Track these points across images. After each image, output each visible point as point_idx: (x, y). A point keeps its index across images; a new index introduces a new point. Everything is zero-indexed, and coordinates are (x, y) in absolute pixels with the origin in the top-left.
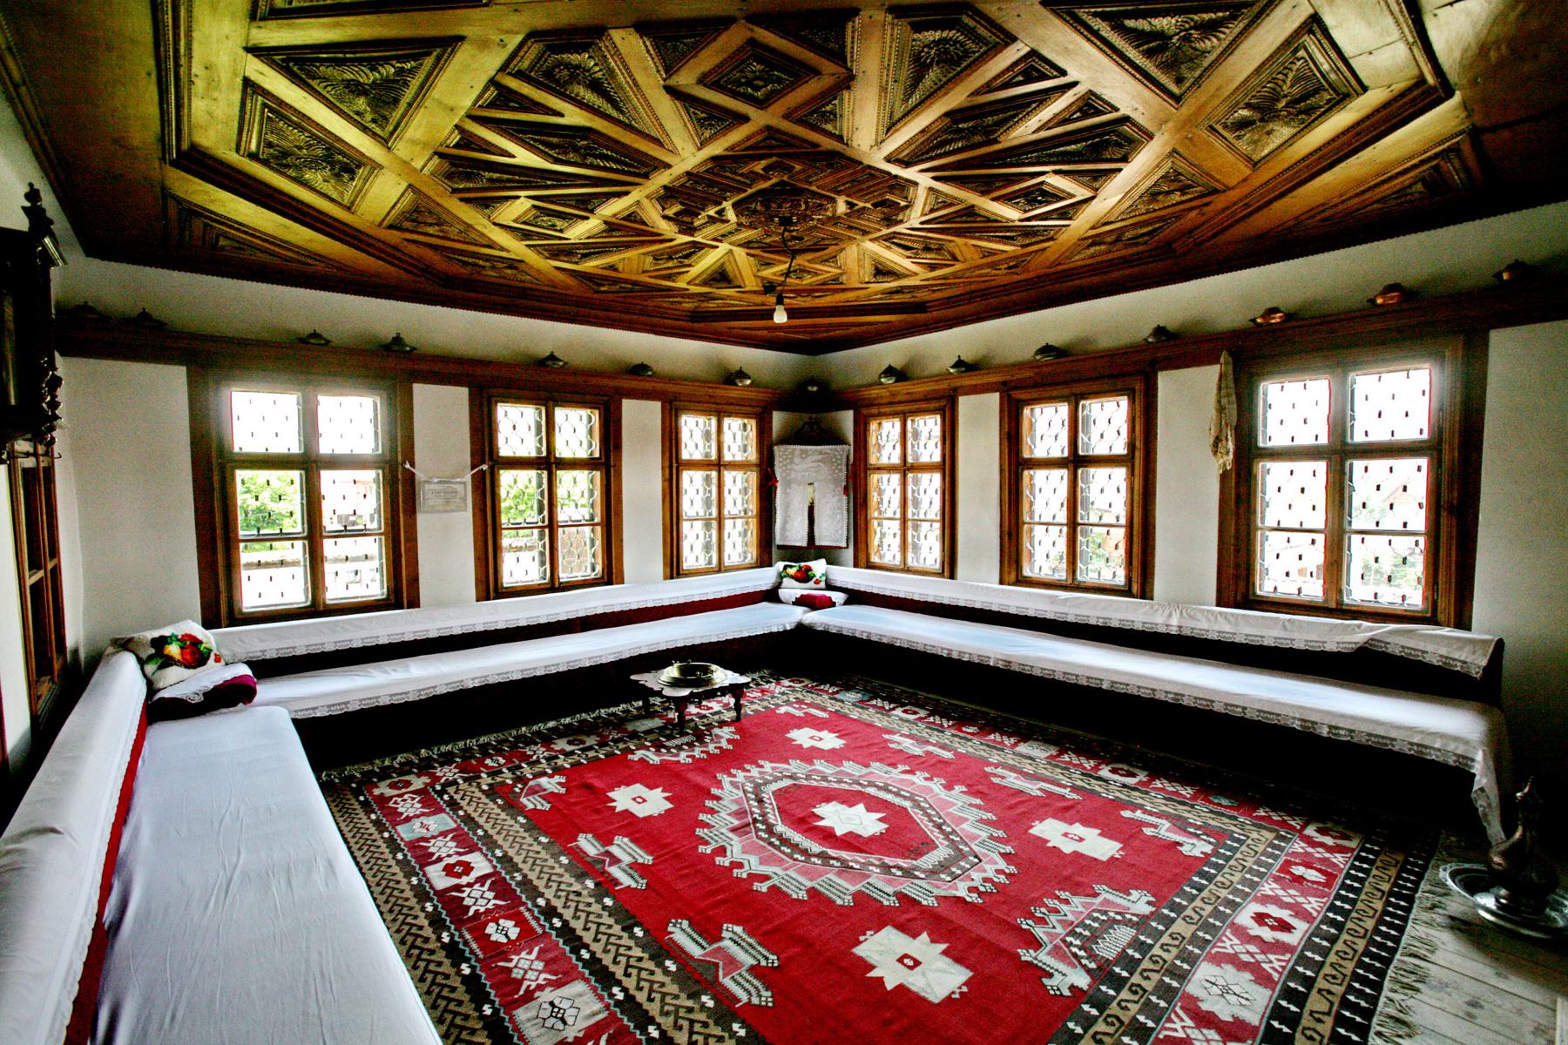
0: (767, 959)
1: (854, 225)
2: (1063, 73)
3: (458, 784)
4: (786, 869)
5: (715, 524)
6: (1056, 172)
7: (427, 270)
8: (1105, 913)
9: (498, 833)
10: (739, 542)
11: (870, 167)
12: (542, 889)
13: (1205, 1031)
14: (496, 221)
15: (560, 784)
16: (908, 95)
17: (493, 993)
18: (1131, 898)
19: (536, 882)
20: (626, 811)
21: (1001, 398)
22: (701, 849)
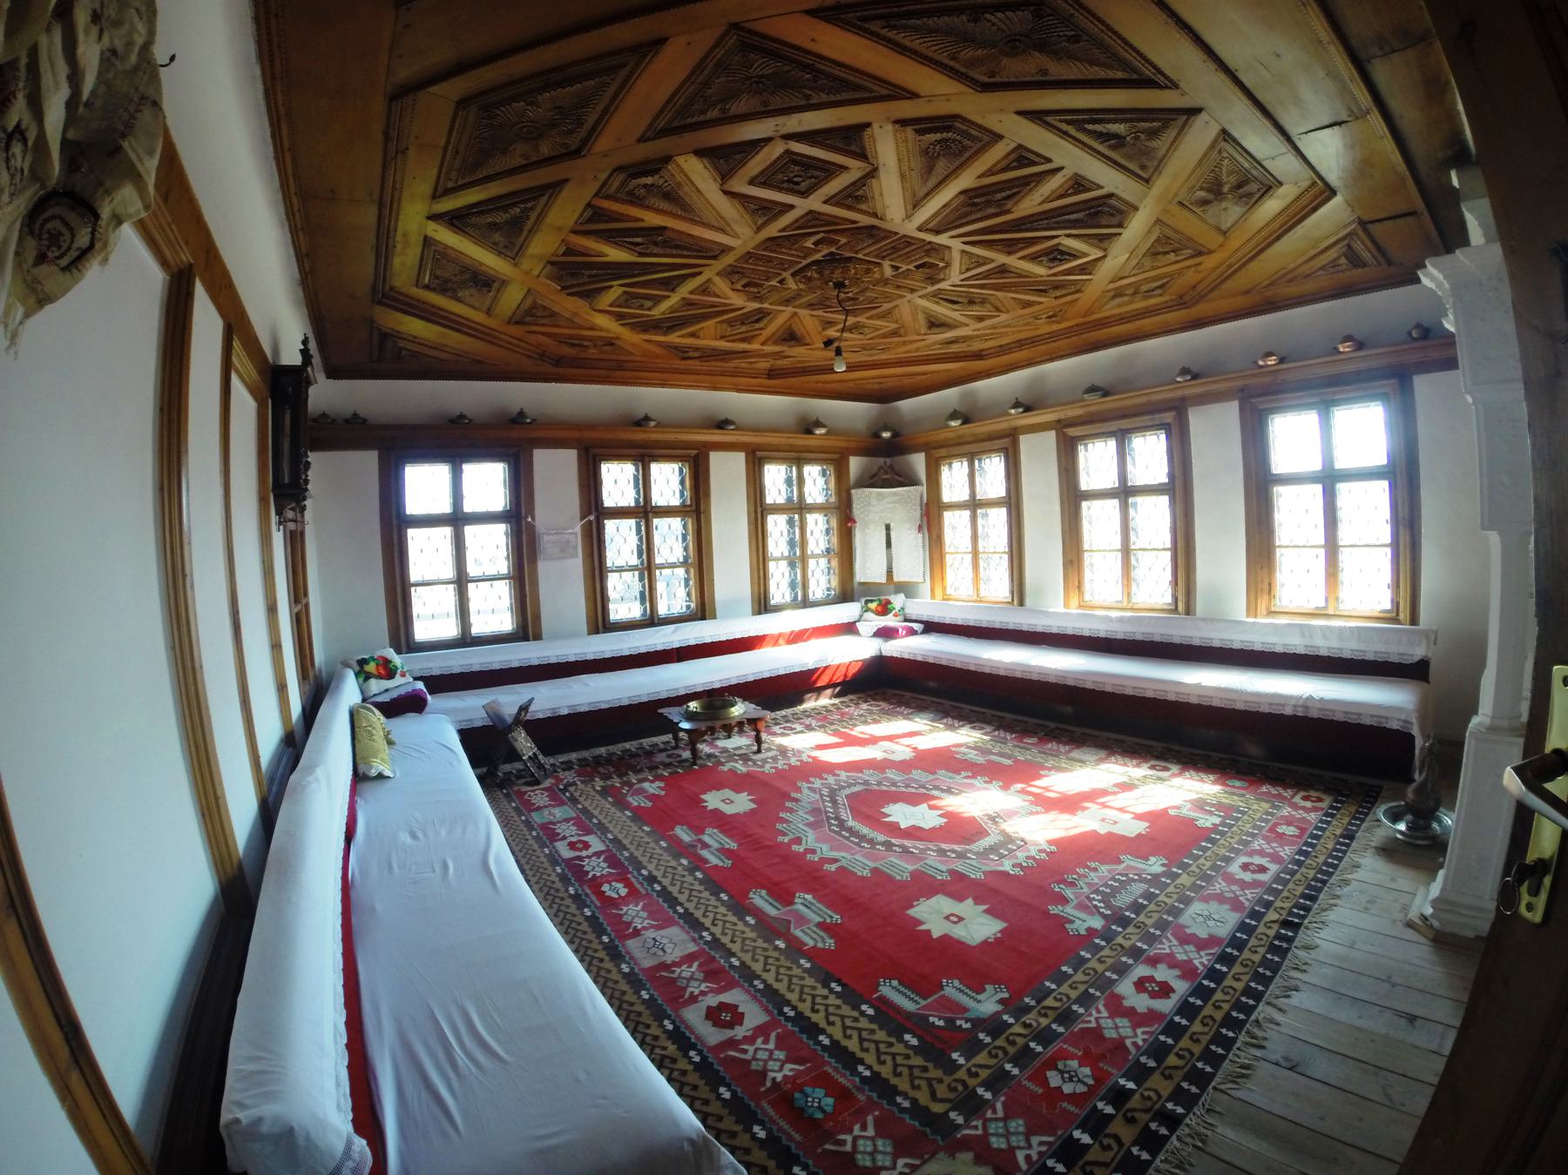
0: (831, 917)
1: (899, 282)
2: (1049, 160)
3: (576, 784)
7: (543, 356)
8: (1126, 875)
9: (610, 822)
10: (821, 580)
11: (905, 236)
12: (645, 864)
13: (1186, 947)
15: (659, 787)
16: (925, 181)
17: (609, 929)
18: (1149, 863)
19: (641, 859)
20: (716, 809)
21: (1057, 435)
22: (780, 839)
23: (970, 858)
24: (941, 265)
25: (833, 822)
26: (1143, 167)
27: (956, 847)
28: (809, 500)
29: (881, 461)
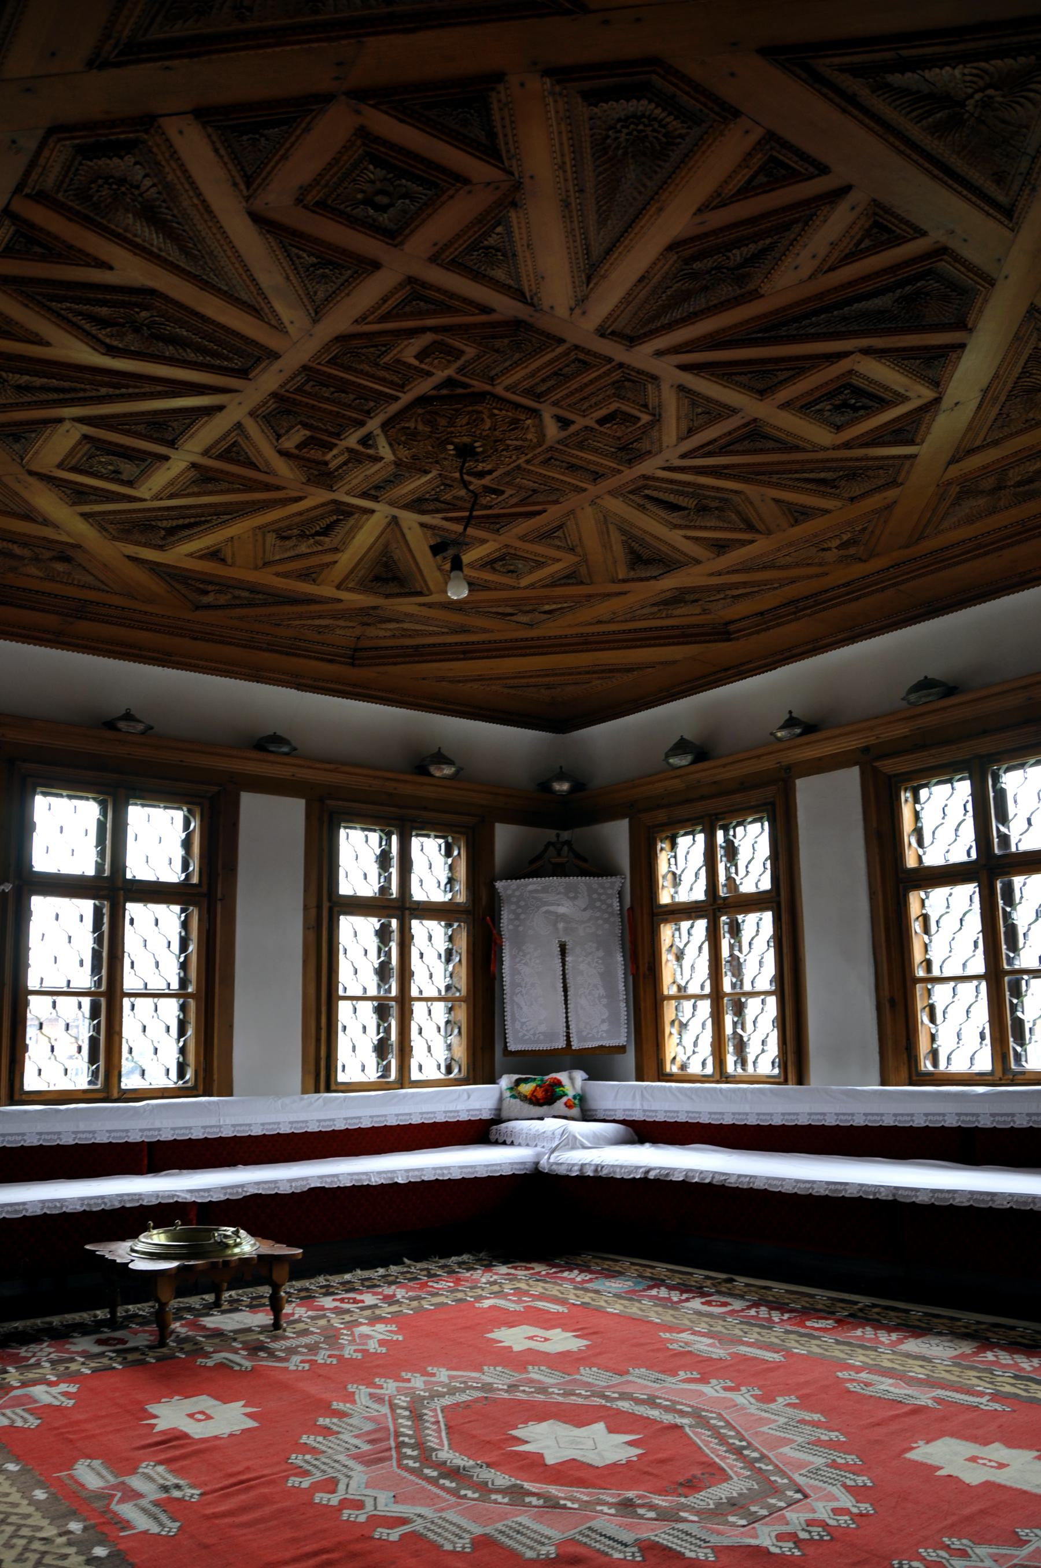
4: (442, 1510)
5: (394, 1011)
6: (867, 352)
14: (34, 467)
21: (863, 774)
22: (293, 1481)
23: (685, 1520)
24: (645, 418)
25: (409, 1452)
26: (999, 178)
27: (658, 1500)
28: (418, 894)
29: (550, 834)
